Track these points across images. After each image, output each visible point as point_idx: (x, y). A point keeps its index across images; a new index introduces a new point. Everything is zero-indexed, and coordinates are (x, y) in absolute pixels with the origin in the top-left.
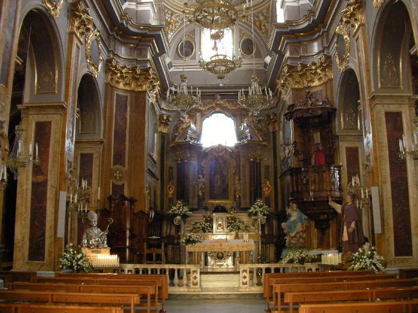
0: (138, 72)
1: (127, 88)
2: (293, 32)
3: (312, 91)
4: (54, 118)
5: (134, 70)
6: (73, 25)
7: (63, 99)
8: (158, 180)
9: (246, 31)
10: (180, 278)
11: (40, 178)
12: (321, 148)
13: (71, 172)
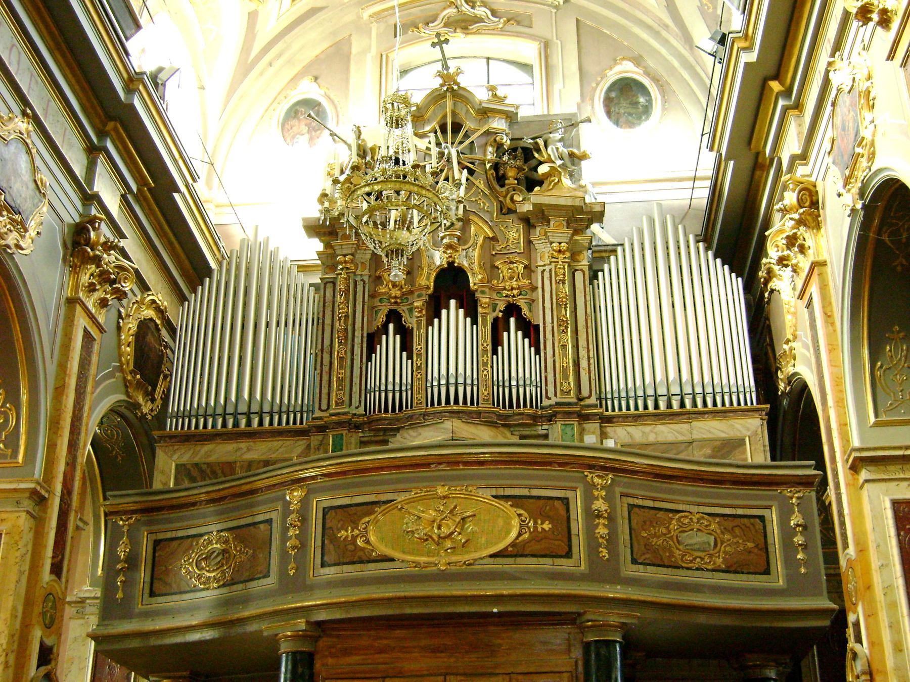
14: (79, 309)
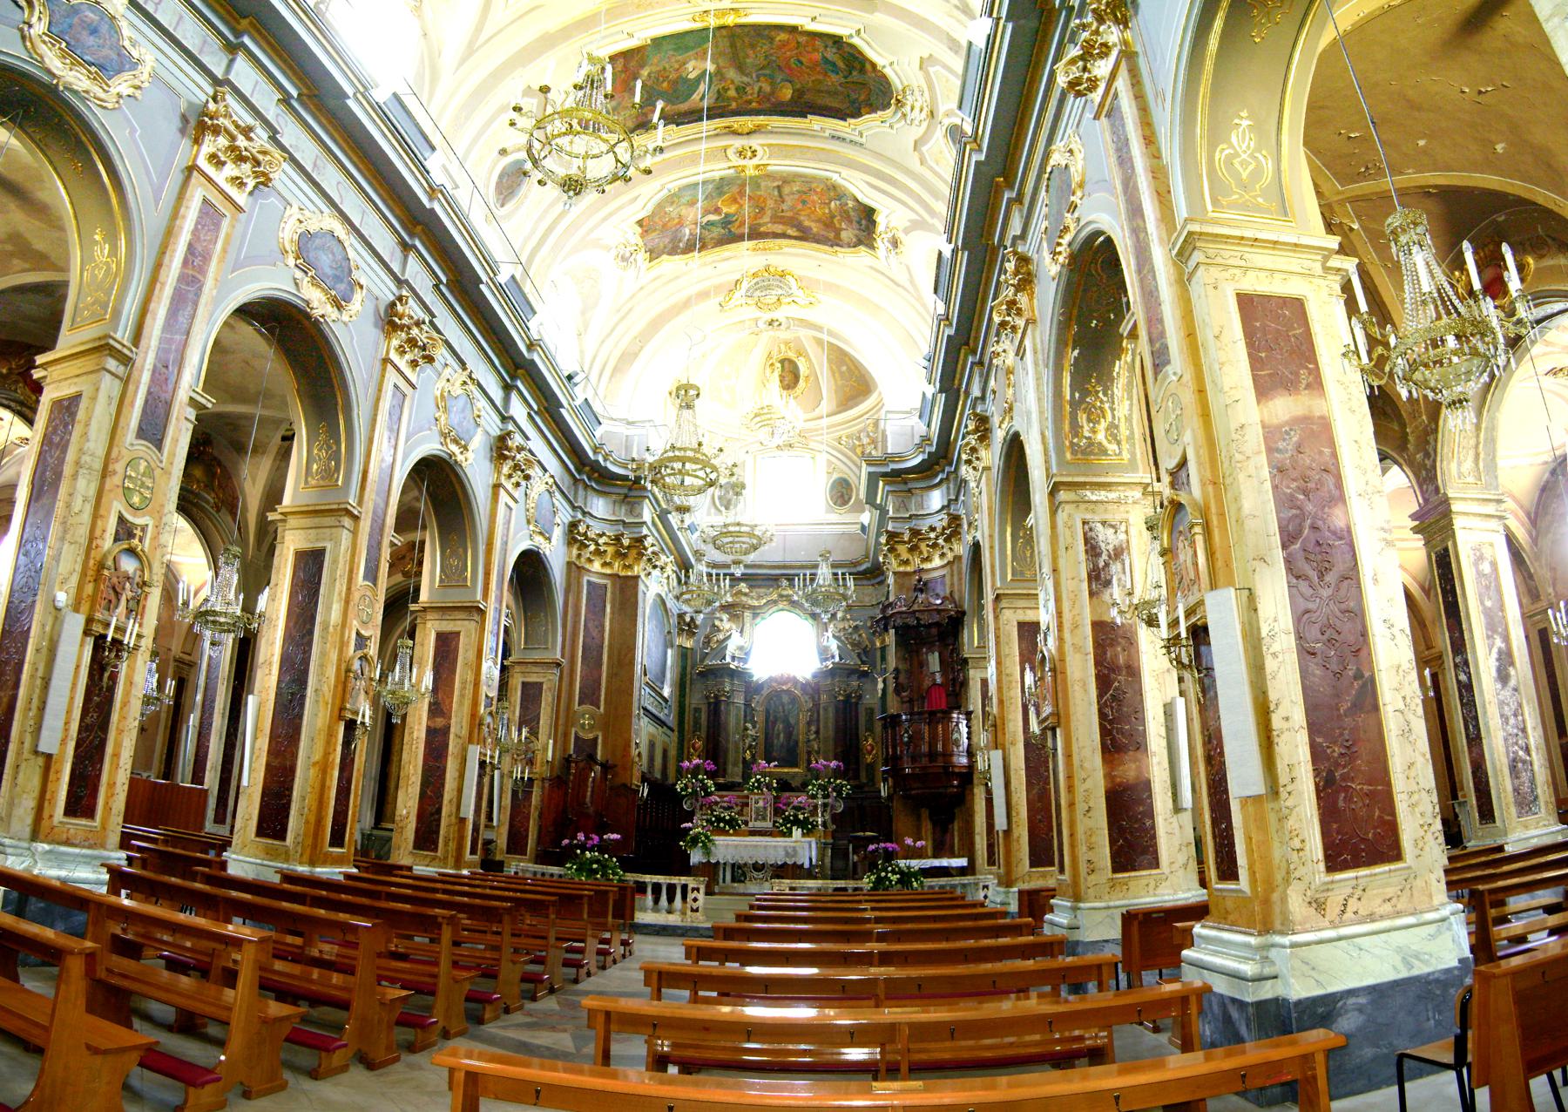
0: (626, 542)
1: (608, 571)
2: (896, 473)
3: (925, 577)
4: (464, 628)
5: (618, 539)
6: (499, 472)
7: (479, 597)
8: (672, 730)
9: (838, 463)
10: (671, 899)
11: (440, 722)
12: (939, 681)
13: (491, 714)
14: (502, 490)
